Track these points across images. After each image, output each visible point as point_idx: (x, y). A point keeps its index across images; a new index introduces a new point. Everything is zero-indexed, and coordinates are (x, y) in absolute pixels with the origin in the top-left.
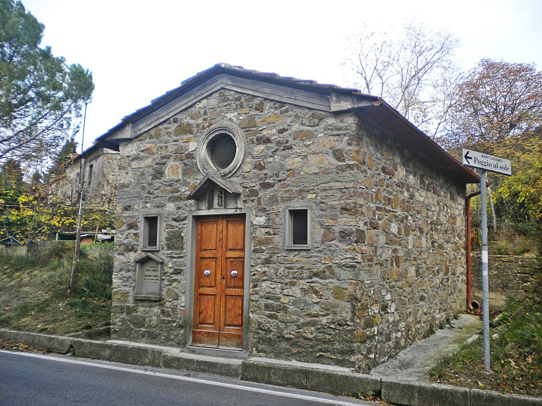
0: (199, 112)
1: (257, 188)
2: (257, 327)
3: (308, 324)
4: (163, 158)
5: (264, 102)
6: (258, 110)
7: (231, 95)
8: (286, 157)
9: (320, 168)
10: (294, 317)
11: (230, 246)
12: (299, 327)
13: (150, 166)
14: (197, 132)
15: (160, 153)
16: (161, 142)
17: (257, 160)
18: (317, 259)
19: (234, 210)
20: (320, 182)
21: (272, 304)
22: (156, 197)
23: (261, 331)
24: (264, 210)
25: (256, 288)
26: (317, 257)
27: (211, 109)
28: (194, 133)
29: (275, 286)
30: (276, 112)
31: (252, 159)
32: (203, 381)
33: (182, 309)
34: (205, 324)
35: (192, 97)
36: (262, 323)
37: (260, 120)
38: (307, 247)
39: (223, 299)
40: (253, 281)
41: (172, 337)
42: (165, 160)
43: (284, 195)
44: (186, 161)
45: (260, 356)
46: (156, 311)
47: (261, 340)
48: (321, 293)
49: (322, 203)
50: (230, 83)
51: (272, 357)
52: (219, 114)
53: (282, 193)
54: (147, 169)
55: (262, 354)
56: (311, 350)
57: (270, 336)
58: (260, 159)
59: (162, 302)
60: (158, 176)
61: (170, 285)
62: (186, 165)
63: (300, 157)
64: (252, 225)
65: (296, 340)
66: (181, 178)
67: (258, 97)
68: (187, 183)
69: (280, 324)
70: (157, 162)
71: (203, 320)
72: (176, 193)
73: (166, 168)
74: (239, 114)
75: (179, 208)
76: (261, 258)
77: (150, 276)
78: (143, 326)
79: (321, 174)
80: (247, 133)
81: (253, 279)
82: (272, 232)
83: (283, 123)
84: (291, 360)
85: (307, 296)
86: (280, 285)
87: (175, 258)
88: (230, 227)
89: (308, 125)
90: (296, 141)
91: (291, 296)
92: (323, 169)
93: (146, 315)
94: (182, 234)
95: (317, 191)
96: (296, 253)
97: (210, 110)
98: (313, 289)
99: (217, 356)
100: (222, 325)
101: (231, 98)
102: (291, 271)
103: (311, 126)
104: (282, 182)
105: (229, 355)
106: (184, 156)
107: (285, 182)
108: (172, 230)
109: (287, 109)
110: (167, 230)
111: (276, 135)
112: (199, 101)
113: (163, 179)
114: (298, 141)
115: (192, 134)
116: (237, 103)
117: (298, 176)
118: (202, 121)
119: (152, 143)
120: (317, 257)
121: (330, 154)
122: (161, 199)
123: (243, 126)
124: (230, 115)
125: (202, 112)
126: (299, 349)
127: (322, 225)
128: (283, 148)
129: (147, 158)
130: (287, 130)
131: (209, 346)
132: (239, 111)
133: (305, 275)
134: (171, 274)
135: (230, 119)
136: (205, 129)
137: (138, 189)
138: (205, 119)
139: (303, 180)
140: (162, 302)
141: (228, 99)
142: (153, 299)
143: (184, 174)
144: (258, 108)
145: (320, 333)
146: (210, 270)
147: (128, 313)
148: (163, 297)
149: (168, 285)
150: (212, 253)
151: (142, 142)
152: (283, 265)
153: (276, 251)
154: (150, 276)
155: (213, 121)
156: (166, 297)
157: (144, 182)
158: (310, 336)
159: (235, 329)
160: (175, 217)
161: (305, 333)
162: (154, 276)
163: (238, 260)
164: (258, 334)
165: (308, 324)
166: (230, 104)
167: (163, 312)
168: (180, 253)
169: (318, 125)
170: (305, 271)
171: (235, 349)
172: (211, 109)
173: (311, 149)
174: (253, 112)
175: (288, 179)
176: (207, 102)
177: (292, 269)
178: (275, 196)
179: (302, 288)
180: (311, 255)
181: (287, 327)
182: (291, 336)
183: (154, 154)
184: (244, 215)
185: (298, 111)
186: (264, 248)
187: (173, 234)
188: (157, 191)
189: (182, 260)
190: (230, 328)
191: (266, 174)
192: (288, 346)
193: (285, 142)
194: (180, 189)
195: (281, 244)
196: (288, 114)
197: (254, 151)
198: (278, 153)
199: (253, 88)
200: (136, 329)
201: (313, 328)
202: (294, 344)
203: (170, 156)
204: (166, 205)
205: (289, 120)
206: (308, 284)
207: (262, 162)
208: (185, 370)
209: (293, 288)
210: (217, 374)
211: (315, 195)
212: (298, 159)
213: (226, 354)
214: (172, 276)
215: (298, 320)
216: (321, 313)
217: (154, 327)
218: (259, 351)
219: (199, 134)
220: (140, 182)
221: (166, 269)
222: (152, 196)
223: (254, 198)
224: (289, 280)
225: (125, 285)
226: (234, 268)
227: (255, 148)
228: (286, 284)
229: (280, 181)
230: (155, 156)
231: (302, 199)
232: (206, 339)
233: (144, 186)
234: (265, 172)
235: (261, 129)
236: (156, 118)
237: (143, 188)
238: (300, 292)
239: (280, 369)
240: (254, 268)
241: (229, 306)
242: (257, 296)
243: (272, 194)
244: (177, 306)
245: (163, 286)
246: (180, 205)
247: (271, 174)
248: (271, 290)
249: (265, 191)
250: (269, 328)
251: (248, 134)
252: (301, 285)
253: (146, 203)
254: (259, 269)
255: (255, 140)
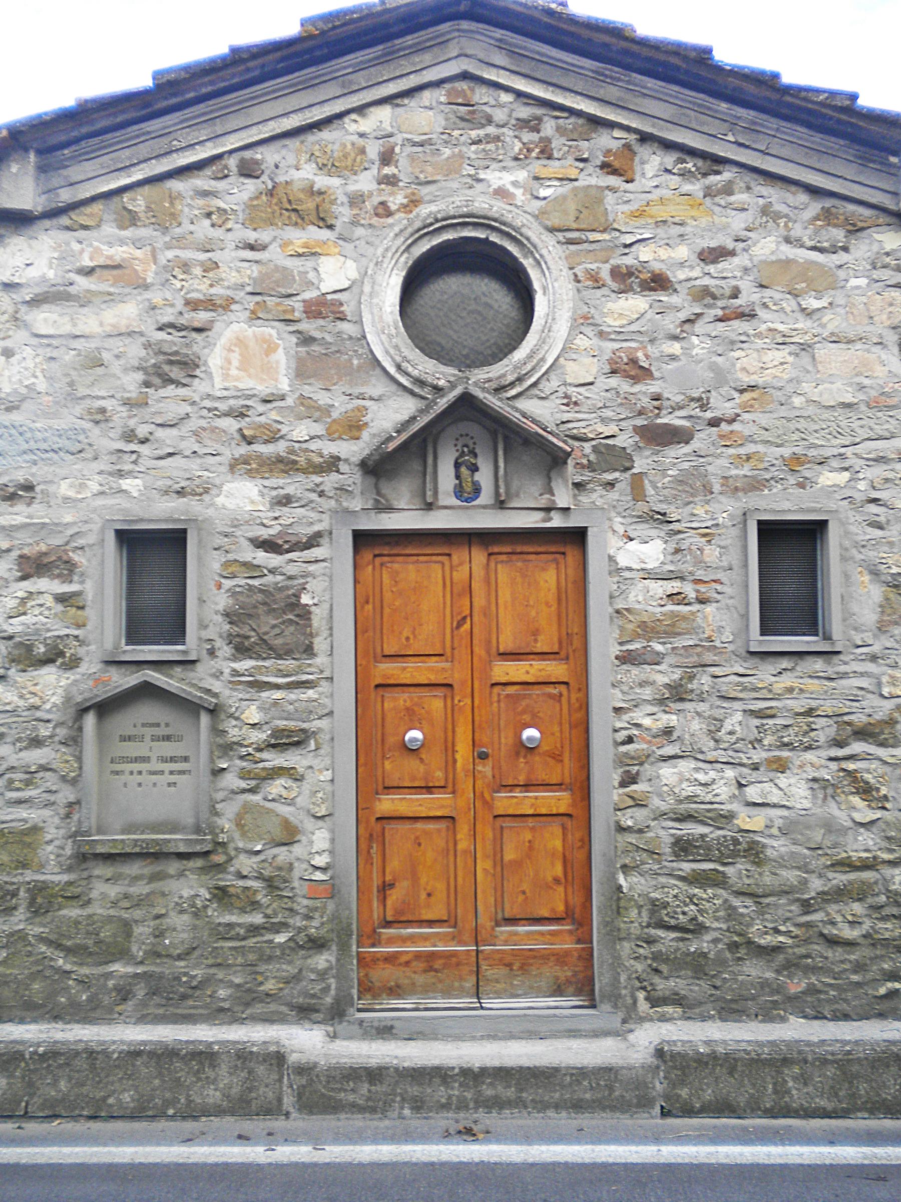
0: (363, 151)
1: (625, 440)
2: (645, 919)
3: (839, 894)
4: (193, 305)
5: (636, 147)
6: (615, 172)
7: (501, 106)
8: (733, 342)
9: (862, 388)
10: (791, 876)
11: (507, 642)
12: (807, 906)
13: (130, 334)
14: (355, 223)
15: (178, 285)
16: (179, 242)
17: (617, 345)
18: (864, 683)
19: (540, 515)
20: (863, 433)
21: (703, 836)
22: (171, 455)
23: (661, 933)
24: (661, 519)
25: (634, 787)
26: (862, 674)
27: (415, 144)
28: (338, 224)
29: (713, 774)
30: (687, 188)
31: (596, 341)
32: (575, 1149)
33: (319, 876)
34: (409, 923)
35: (332, 90)
36: (666, 905)
37: (626, 208)
38: (184, 652)
39: (487, 832)
40: (621, 761)
41: (270, 986)
42: (202, 317)
43: (734, 472)
44: (309, 327)
45: (663, 1019)
46: (186, 893)
47: (667, 960)
48: (884, 791)
49: (875, 501)
50: (500, 59)
51: (711, 1017)
52: (451, 169)
53: (724, 462)
54: (117, 345)
55: (669, 1009)
56: (855, 978)
57: (703, 944)
58: (633, 345)
59: (219, 858)
60: (175, 373)
61: (252, 791)
62: (307, 340)
63: (788, 349)
64: (615, 570)
65: (802, 951)
66: (284, 385)
67: (612, 125)
68: (319, 408)
69: (736, 902)
70: (166, 319)
71: (398, 912)
72: (266, 442)
73: (210, 345)
74: (537, 178)
75: (285, 501)
76: (653, 683)
77: (145, 759)
78: (122, 954)
79: (863, 407)
80: (572, 248)
81: (626, 754)
82: (693, 595)
83: (712, 228)
84: (783, 1019)
85: (833, 805)
86: (730, 773)
87: (278, 687)
88: (503, 573)
89: (810, 243)
90: (767, 293)
91: (775, 806)
92: (874, 393)
93: (138, 914)
94: (305, 599)
95: (858, 463)
96: (785, 663)
97: (409, 149)
98: (855, 780)
99: (492, 1037)
100: (485, 920)
101: (499, 115)
102: (771, 722)
103: (821, 250)
104: (723, 425)
105: (543, 1028)
106: (299, 306)
107: (736, 426)
108: (255, 583)
109: (730, 182)
110: (227, 584)
111: (692, 267)
112: (361, 110)
113: (200, 387)
114: (778, 296)
115: (331, 227)
116: (527, 136)
117: (783, 412)
118: (374, 186)
119: (137, 244)
120: (862, 674)
121: (890, 344)
122: (194, 466)
123: (555, 220)
124: (496, 178)
125: (373, 150)
126: (813, 980)
127: (875, 573)
128: (720, 313)
129: (110, 299)
130: (732, 253)
131: (441, 1002)
132: (537, 167)
133: (822, 737)
134: (259, 750)
135: (501, 193)
136: (389, 214)
137: (69, 419)
138: (391, 181)
139: (802, 424)
140: (219, 858)
141: (489, 120)
142: (182, 849)
143: (301, 373)
144: (616, 164)
145: (883, 919)
146: (420, 729)
147: (36, 911)
148: (222, 838)
149: (244, 791)
150: (430, 669)
151: (81, 234)
152: (737, 705)
153: (709, 658)
154: (145, 759)
155: (425, 191)
156: (237, 835)
157: (103, 393)
158: (849, 933)
159: (542, 934)
160: (264, 533)
161: (833, 923)
162: (164, 760)
163: (537, 691)
164: (650, 941)
165: (839, 894)
166: (497, 138)
167: (221, 895)
168: (299, 671)
169: (845, 249)
170: (822, 722)
171: (551, 1001)
172: (415, 144)
173: (823, 326)
174: (593, 179)
175: (746, 416)
176: (394, 118)
177: (773, 716)
178: (698, 473)
179: (814, 780)
180: (842, 668)
181: (762, 910)
182: (781, 939)
183: (146, 287)
184: (578, 536)
185: (774, 195)
186: (659, 648)
187: (260, 597)
188: (174, 432)
189: (311, 693)
190: (520, 929)
191: (657, 398)
192: (770, 975)
193: (728, 292)
194: (284, 430)
195: (727, 636)
196: (732, 199)
197: (604, 315)
198: (699, 327)
199: (601, 94)
200: (85, 970)
201: (857, 908)
202: (791, 966)
203: (231, 301)
204: (219, 487)
205: (738, 222)
206: (834, 766)
207: (640, 354)
208: (407, 1112)
209: (783, 780)
210: (557, 1107)
211: (846, 475)
212: (782, 354)
213: (531, 1026)
214: (265, 755)
215: (805, 882)
216: (886, 856)
217: (179, 958)
218: (654, 1002)
219: (360, 232)
220: (82, 391)
221: (235, 731)
222: (144, 449)
223: (617, 475)
224: (765, 755)
225: (20, 802)
226: (527, 718)
227: (610, 305)
228: (755, 767)
229: (714, 423)
230: (156, 297)
231: (801, 486)
232: (420, 979)
233: (103, 411)
234: (654, 387)
235: (629, 239)
236: (162, 144)
237: (100, 417)
238: (808, 793)
239: (824, 1062)
240: (626, 717)
241: (509, 855)
242: (640, 814)
243: (686, 465)
244: (291, 867)
245: (220, 795)
246: (290, 490)
247: (679, 398)
248: (698, 790)
249: (657, 453)
250: (694, 919)
251: (577, 253)
252: (808, 768)
253: (120, 474)
254: (647, 722)
255: (605, 275)
